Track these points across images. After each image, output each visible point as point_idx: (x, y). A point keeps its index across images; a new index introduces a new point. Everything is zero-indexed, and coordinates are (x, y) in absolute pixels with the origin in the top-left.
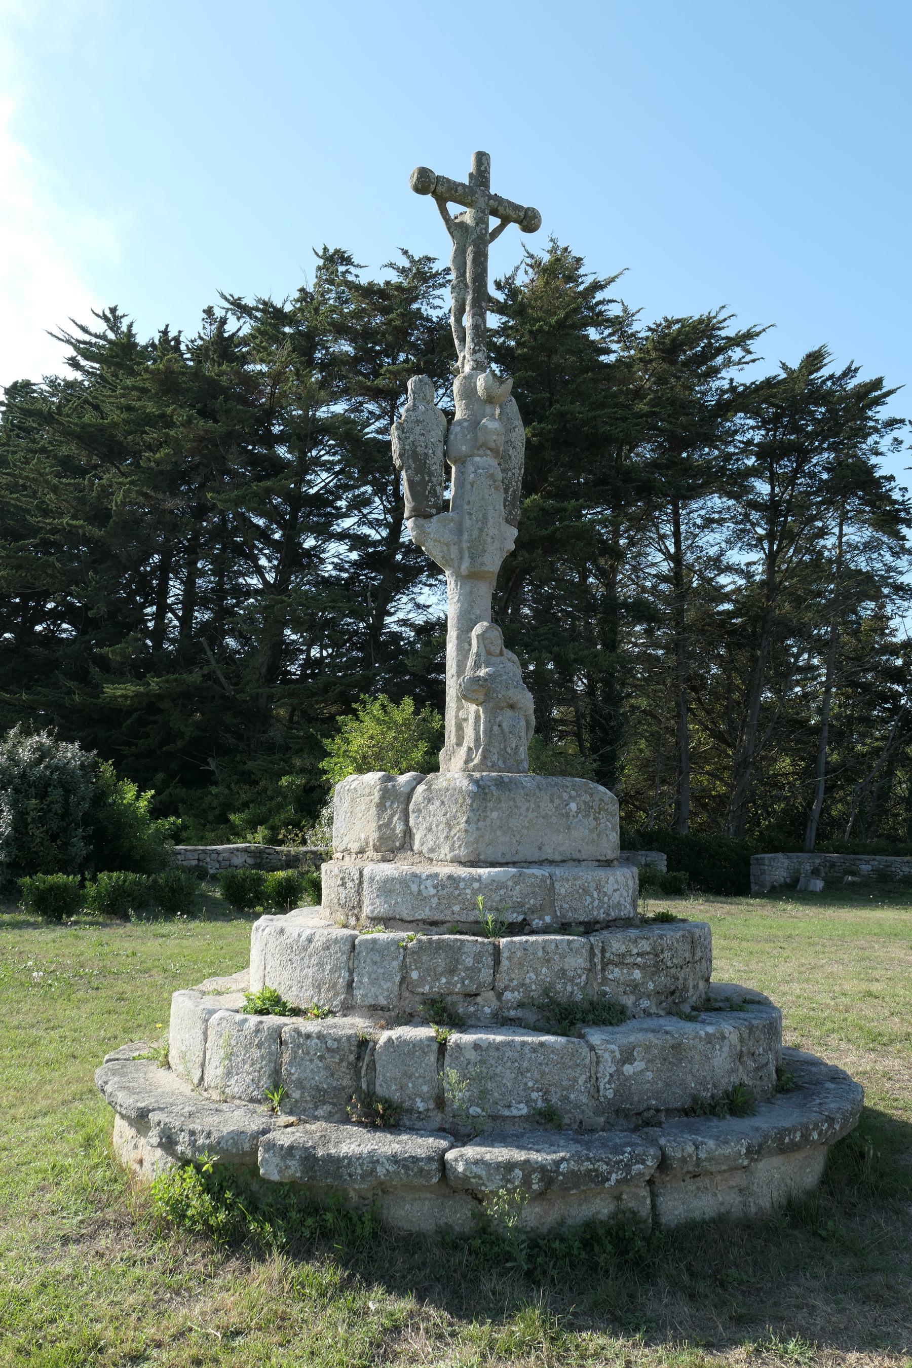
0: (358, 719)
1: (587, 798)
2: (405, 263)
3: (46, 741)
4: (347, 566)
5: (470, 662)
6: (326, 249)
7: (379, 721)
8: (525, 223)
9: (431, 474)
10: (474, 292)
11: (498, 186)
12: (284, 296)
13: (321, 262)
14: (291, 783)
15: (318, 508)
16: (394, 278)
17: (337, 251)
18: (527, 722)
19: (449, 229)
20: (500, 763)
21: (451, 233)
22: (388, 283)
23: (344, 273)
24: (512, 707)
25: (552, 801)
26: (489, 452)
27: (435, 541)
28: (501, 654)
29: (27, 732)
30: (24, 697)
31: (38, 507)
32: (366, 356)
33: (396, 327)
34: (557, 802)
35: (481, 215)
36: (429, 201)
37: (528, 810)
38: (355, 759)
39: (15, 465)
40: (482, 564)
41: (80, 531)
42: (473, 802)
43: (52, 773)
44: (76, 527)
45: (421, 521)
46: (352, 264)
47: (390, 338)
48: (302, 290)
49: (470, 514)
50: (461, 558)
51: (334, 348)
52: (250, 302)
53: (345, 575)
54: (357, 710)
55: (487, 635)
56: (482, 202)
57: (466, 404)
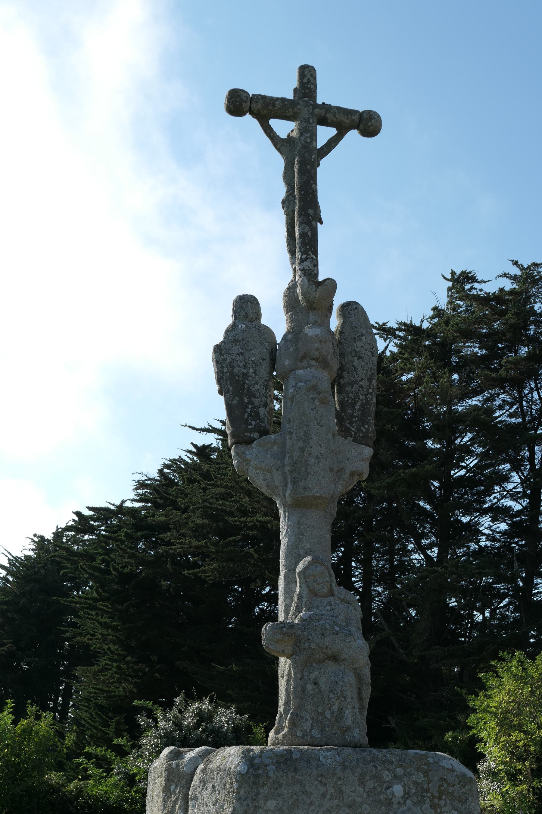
0: (497, 676)
1: (420, 777)
2: (517, 271)
3: (206, 705)
4: (498, 536)
5: (293, 607)
6: (453, 273)
7: (515, 677)
8: (362, 126)
9: (251, 395)
10: (300, 201)
11: (325, 94)
12: (419, 315)
13: (450, 284)
14: (455, 739)
15: (471, 489)
16: (508, 285)
17: (463, 273)
18: (359, 678)
19: (275, 145)
20: (315, 733)
21: (279, 150)
22: (501, 290)
23: (470, 290)
24: (334, 658)
25: (362, 784)
26: (313, 363)
27: (256, 468)
28: (331, 593)
29: (190, 698)
30: (235, 668)
31: (238, 509)
32: (494, 354)
33: (512, 325)
34: (370, 784)
35: (304, 124)
36: (249, 121)
37: (323, 796)
38: (495, 714)
39: (216, 477)
40: (305, 488)
41: (269, 525)
42: (240, 787)
43: (208, 736)
44: (264, 522)
45: (242, 448)
46: (476, 281)
47: (508, 335)
48: (435, 309)
49: (291, 433)
50: (286, 485)
51: (467, 351)
52: (393, 324)
53: (498, 545)
54: (495, 667)
55: (309, 572)
56: (305, 112)
57: (291, 316)
